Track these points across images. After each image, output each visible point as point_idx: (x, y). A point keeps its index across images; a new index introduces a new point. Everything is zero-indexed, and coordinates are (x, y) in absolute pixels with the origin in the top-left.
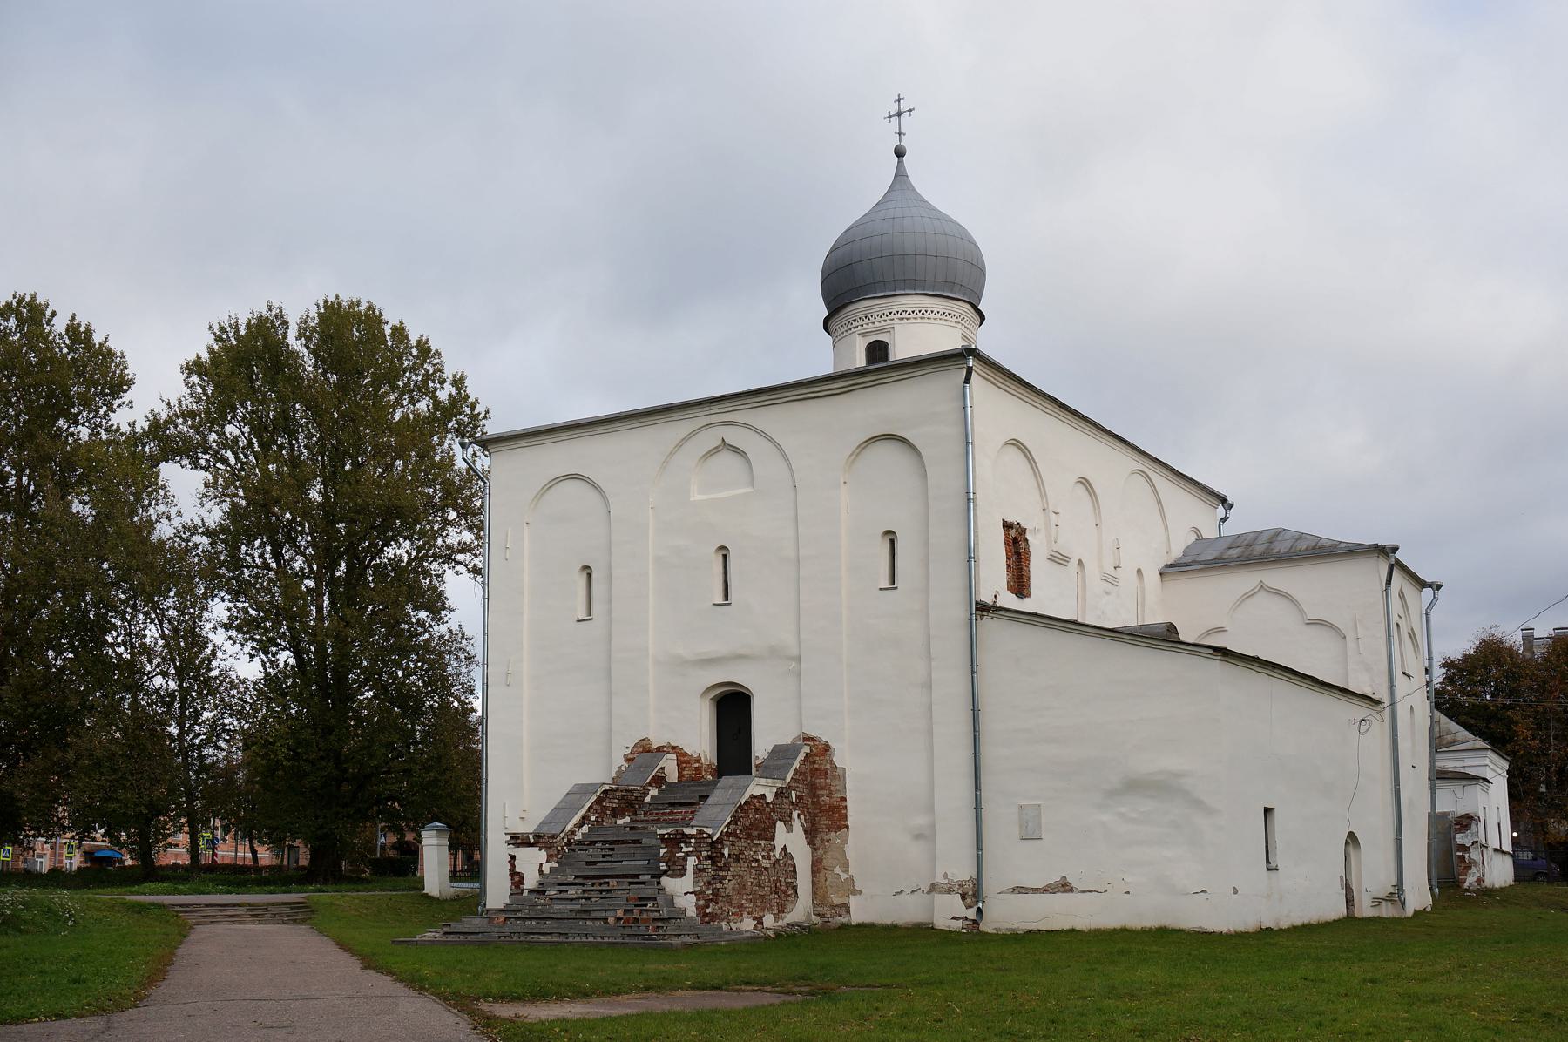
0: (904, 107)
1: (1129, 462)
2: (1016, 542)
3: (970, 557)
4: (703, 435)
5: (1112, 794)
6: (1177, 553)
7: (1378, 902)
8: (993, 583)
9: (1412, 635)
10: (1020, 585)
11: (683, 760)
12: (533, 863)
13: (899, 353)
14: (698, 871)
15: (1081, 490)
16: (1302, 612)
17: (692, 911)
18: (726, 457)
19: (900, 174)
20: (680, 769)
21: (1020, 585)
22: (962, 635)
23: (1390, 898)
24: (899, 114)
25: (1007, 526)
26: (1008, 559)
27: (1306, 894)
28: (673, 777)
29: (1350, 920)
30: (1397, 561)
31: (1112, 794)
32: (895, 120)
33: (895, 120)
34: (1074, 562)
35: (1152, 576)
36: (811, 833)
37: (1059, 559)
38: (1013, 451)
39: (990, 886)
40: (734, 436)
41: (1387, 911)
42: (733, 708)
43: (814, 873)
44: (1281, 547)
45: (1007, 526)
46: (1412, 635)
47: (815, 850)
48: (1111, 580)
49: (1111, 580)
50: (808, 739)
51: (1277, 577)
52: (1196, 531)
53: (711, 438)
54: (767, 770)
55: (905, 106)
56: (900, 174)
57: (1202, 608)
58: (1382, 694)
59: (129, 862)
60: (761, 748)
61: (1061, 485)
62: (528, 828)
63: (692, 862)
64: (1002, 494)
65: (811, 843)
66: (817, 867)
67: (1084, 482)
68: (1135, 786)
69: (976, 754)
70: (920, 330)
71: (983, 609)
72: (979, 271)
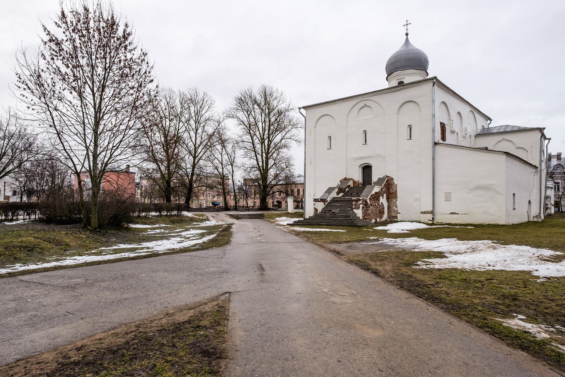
0: (408, 23)
3: (434, 131)
4: (360, 104)
5: (472, 190)
6: (479, 132)
7: (534, 217)
8: (438, 138)
10: (443, 138)
11: (354, 182)
12: (320, 206)
14: (363, 208)
15: (443, 105)
16: (515, 145)
17: (361, 218)
18: (366, 108)
19: (407, 40)
20: (354, 184)
21: (443, 138)
23: (537, 217)
25: (441, 123)
28: (352, 186)
31: (472, 190)
32: (406, 26)
33: (406, 26)
35: (473, 137)
36: (388, 199)
37: (453, 132)
39: (437, 210)
40: (368, 103)
41: (535, 220)
42: (367, 169)
43: (388, 209)
44: (508, 130)
45: (441, 123)
47: (388, 203)
50: (387, 176)
51: (507, 137)
52: (483, 126)
54: (376, 183)
56: (407, 40)
58: (538, 165)
60: (375, 179)
62: (318, 197)
63: (361, 206)
65: (388, 201)
66: (389, 207)
68: (478, 188)
70: (410, 76)
71: (436, 144)
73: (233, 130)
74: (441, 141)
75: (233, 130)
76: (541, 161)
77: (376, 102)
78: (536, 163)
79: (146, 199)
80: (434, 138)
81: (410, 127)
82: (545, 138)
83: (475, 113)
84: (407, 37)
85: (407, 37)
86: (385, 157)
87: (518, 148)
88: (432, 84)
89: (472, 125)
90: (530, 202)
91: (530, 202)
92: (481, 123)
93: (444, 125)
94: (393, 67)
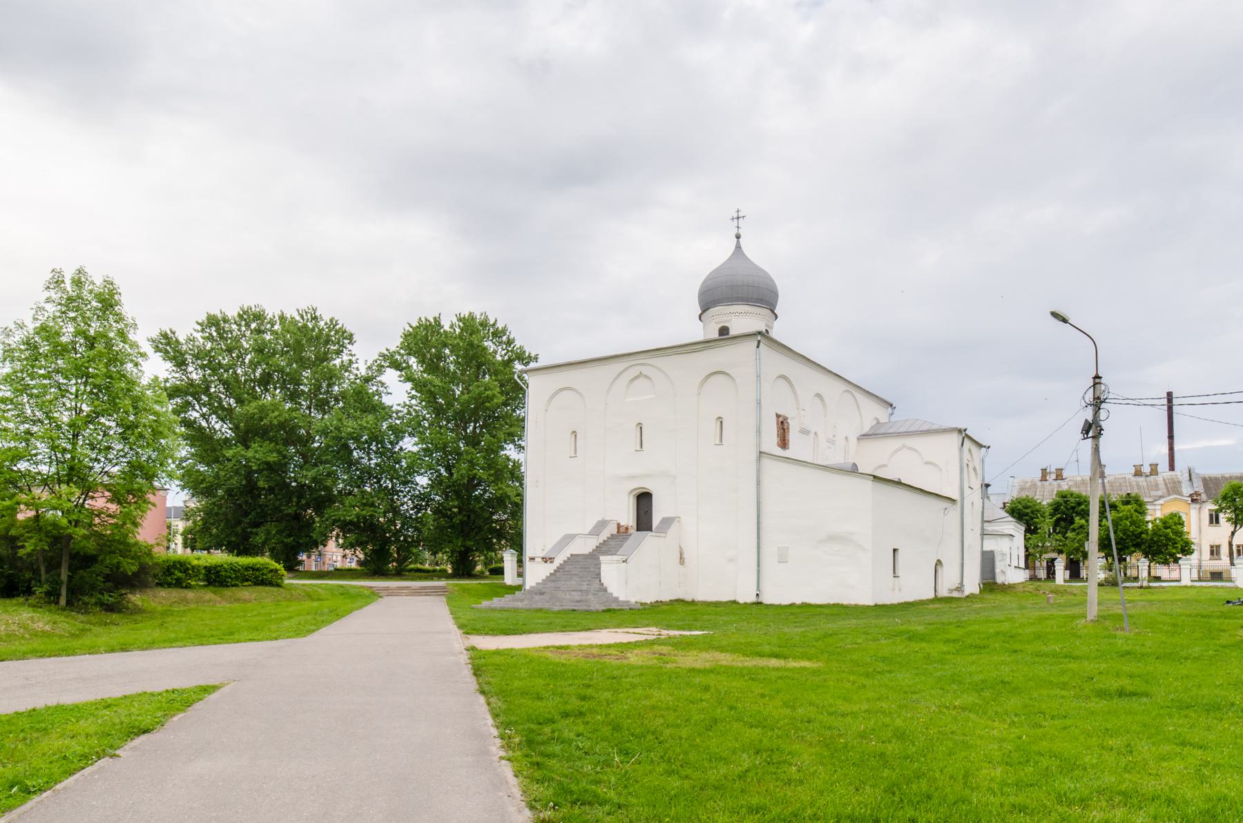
1: (843, 387)
2: (783, 426)
6: (866, 430)
7: (951, 591)
8: (770, 441)
9: (975, 469)
10: (784, 443)
13: (732, 332)
15: (817, 400)
18: (642, 380)
19: (738, 247)
21: (784, 443)
22: (754, 466)
25: (778, 416)
26: (92, 650)
27: (915, 586)
29: (937, 600)
30: (967, 436)
34: (812, 434)
35: (853, 440)
37: (805, 432)
38: (782, 381)
41: (956, 594)
42: (644, 500)
45: (778, 416)
46: (975, 469)
48: (832, 442)
53: (634, 372)
55: (741, 214)
56: (738, 247)
57: (874, 457)
58: (956, 496)
67: (818, 395)
68: (831, 538)
70: (743, 320)
72: (775, 295)
73: (397, 393)
74: (779, 451)
75: (397, 393)
77: (659, 369)
80: (759, 444)
81: (720, 421)
84: (738, 243)
85: (738, 243)
87: (927, 463)
93: (786, 419)
94: (713, 297)
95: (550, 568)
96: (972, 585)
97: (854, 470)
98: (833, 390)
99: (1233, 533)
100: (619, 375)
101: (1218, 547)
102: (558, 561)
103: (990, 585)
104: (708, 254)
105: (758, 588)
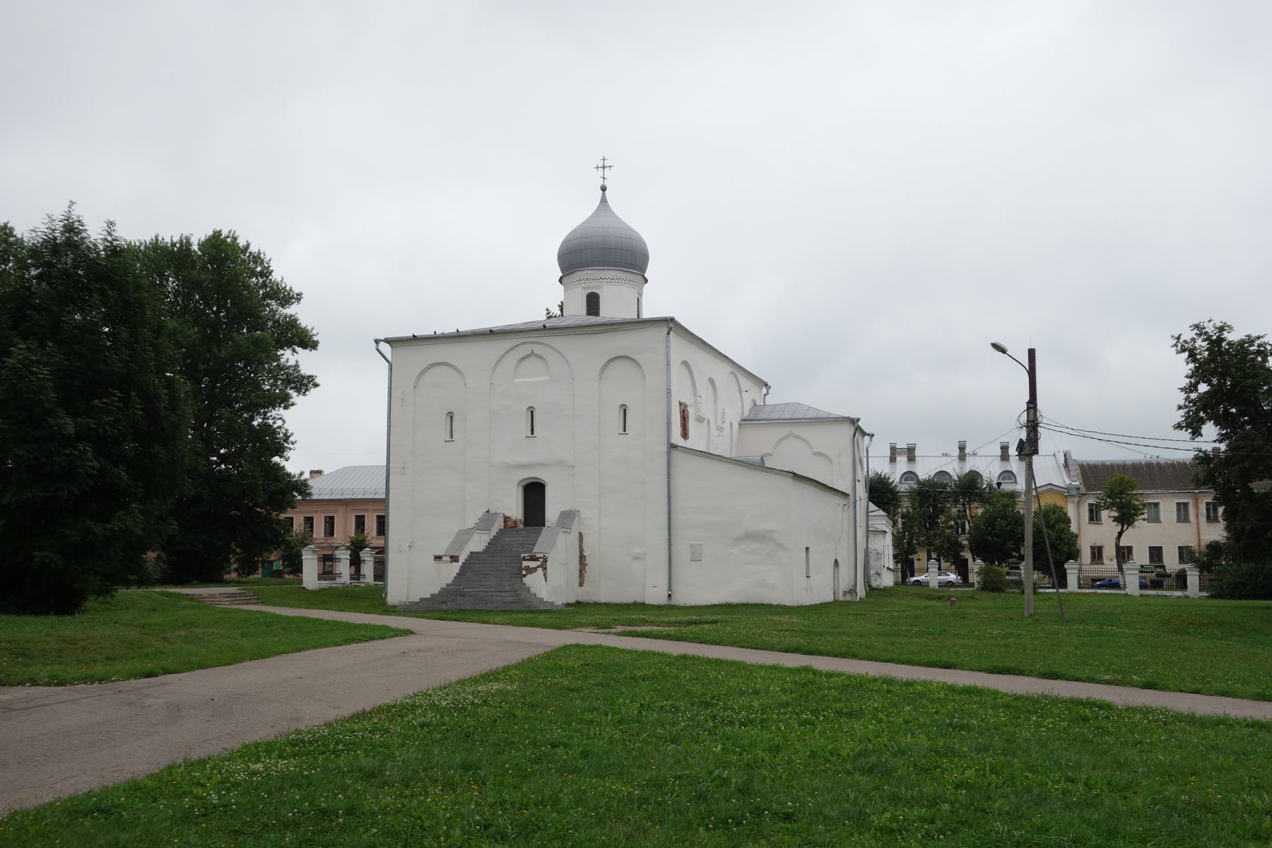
1: (729, 369)
5: (738, 539)
7: (845, 593)
10: (685, 434)
15: (683, 367)
18: (533, 360)
19: (604, 200)
21: (685, 434)
24: (604, 167)
25: (681, 404)
29: (836, 601)
31: (738, 539)
35: (736, 426)
37: (700, 420)
40: (538, 349)
41: (848, 598)
42: (534, 493)
48: (720, 429)
49: (720, 429)
51: (798, 431)
52: (754, 401)
53: (525, 350)
55: (607, 163)
56: (604, 200)
57: (760, 443)
58: (848, 491)
59: (980, 511)
61: (702, 383)
64: (681, 393)
68: (749, 536)
69: (669, 519)
76: (855, 481)
77: (555, 349)
78: (845, 486)
79: (273, 558)
82: (864, 434)
83: (740, 376)
86: (573, 467)
88: (666, 330)
89: (733, 405)
90: (836, 562)
91: (836, 562)
92: (754, 394)
93: (686, 406)
95: (456, 568)
96: (861, 591)
97: (759, 466)
98: (721, 373)
99: (1120, 534)
100: (507, 352)
101: (1100, 549)
102: (462, 559)
103: (871, 590)
104: (570, 215)
105: (670, 589)
